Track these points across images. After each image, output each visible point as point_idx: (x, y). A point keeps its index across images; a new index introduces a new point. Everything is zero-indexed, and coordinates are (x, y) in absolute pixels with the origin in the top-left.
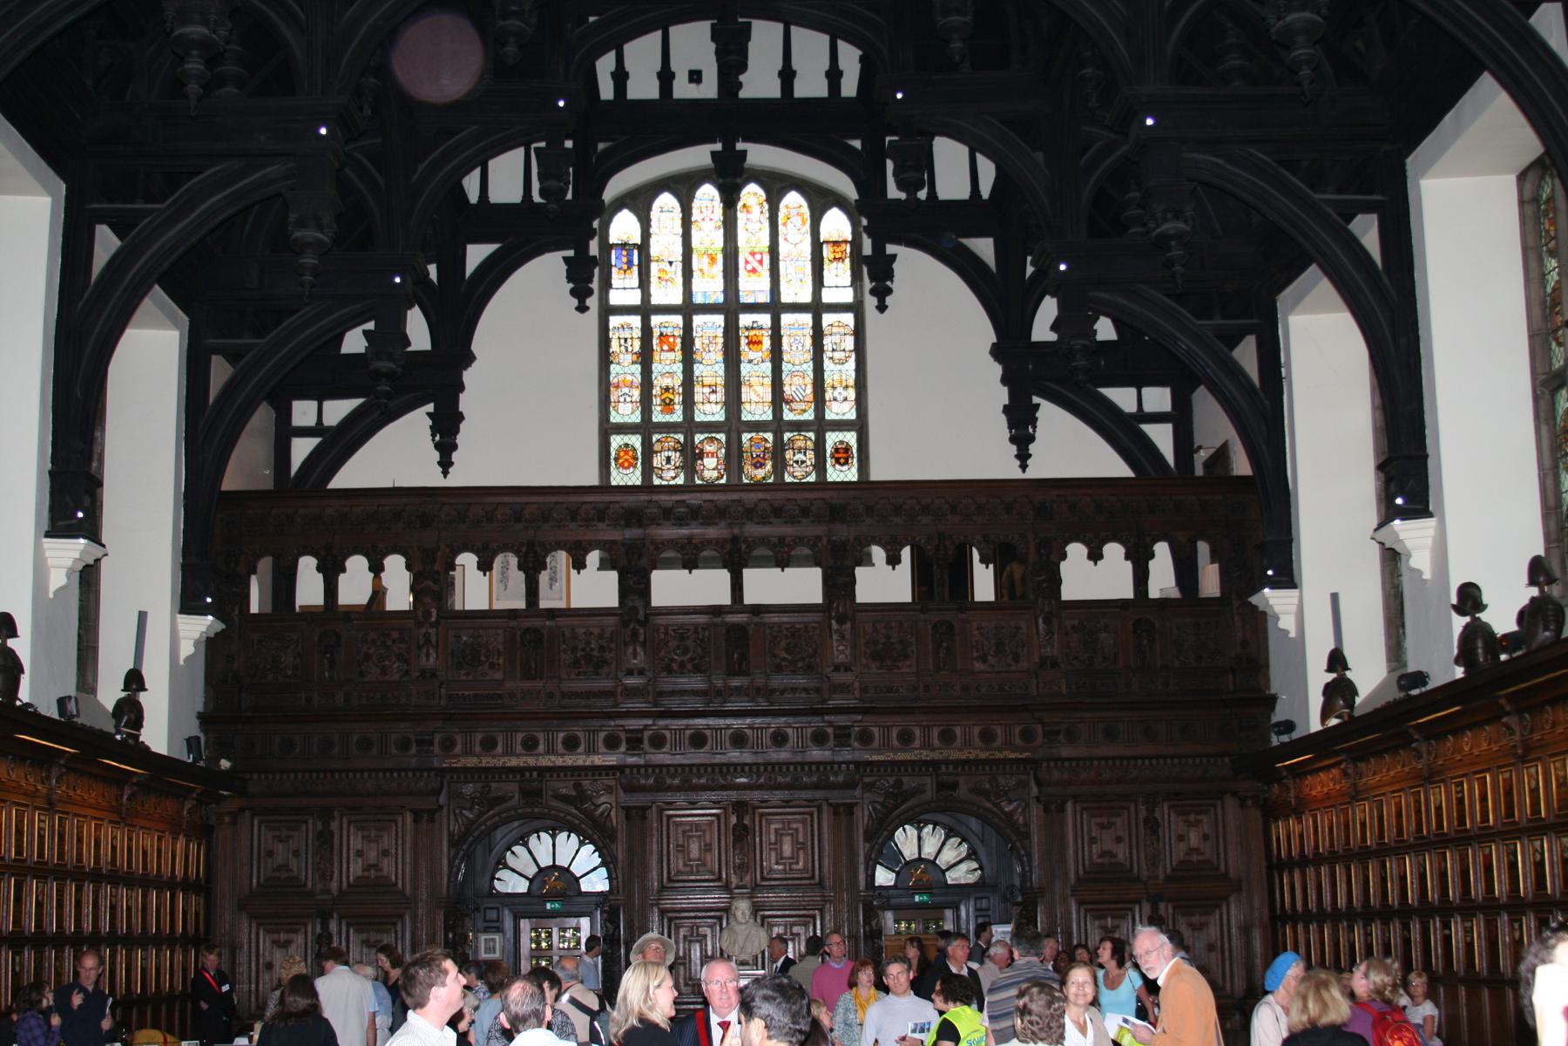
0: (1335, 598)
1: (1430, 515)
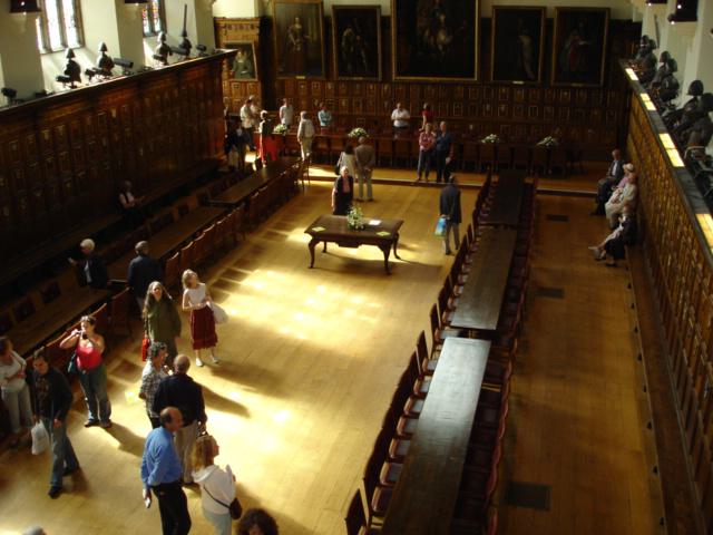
0: (186, 6)
1: (548, 509)
